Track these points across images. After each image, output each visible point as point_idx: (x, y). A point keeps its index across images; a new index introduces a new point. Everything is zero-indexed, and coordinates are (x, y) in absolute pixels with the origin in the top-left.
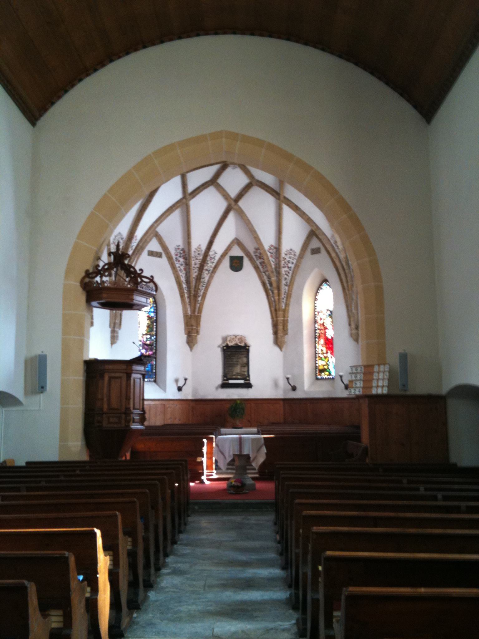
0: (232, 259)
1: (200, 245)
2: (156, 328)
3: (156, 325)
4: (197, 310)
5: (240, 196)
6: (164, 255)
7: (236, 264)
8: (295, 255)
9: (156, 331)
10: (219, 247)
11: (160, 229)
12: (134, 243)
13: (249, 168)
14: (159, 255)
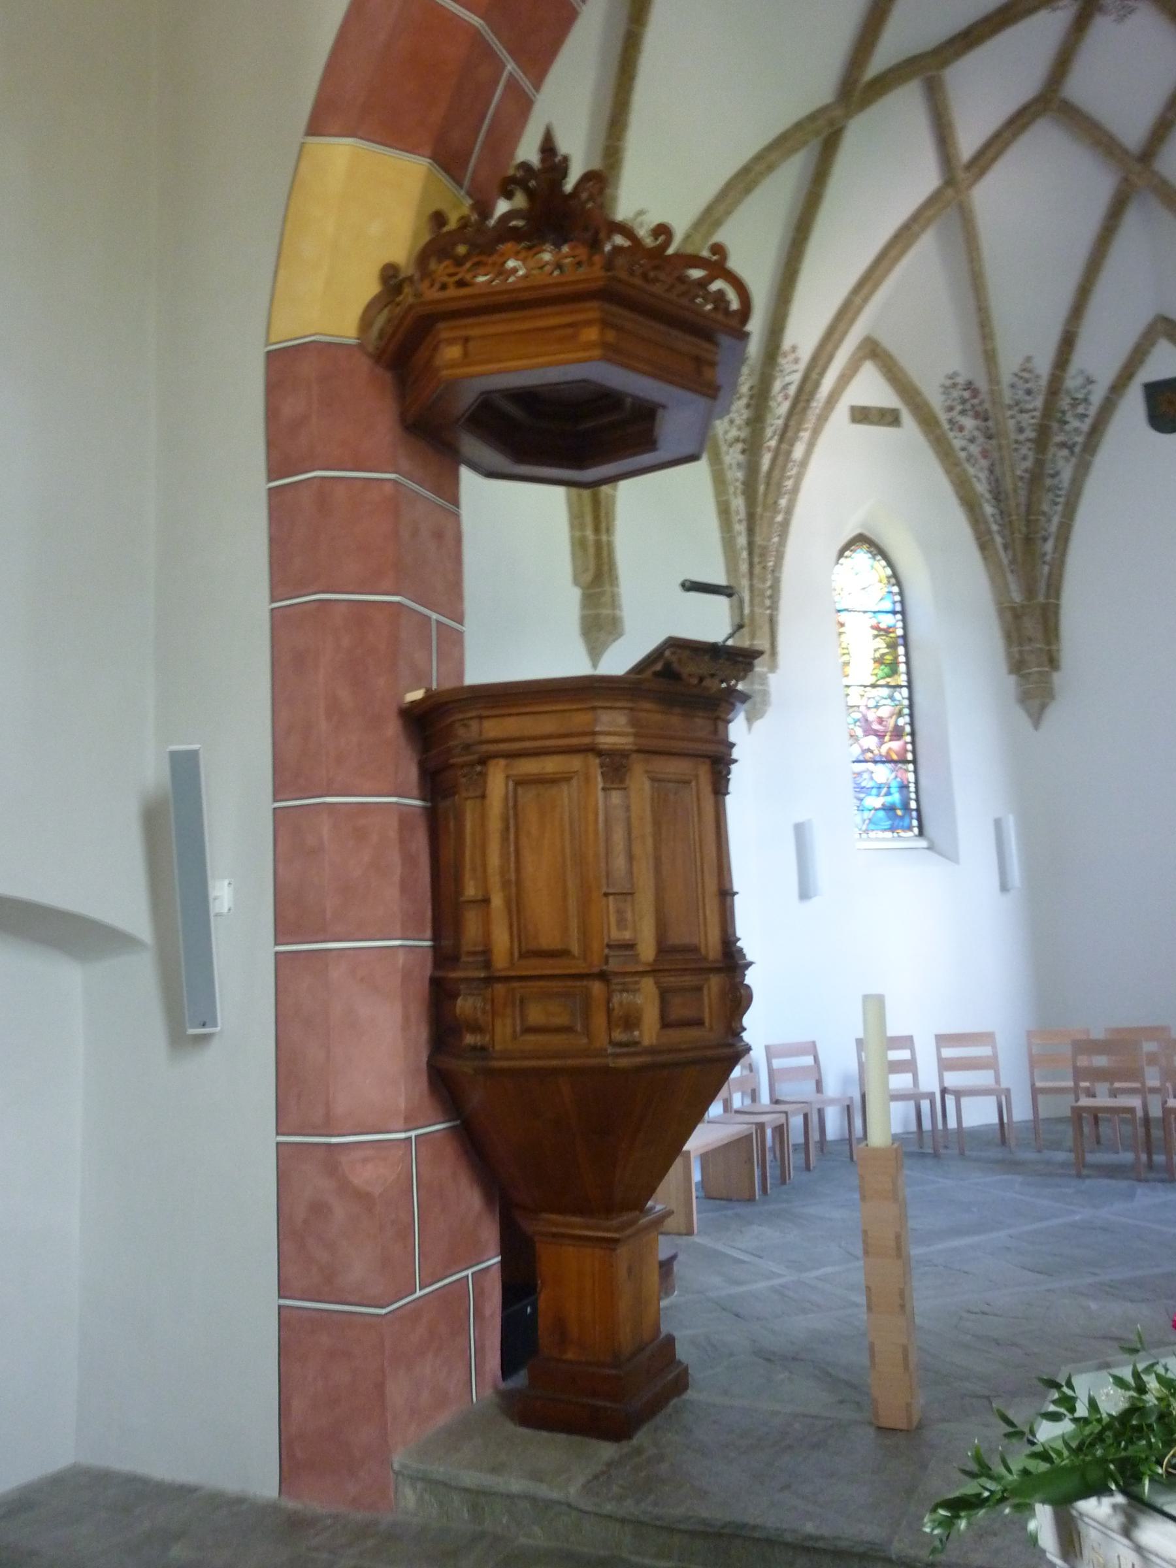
1: (1029, 359)
2: (907, 663)
3: (907, 655)
4: (1042, 585)
6: (906, 417)
9: (908, 673)
10: (1098, 359)
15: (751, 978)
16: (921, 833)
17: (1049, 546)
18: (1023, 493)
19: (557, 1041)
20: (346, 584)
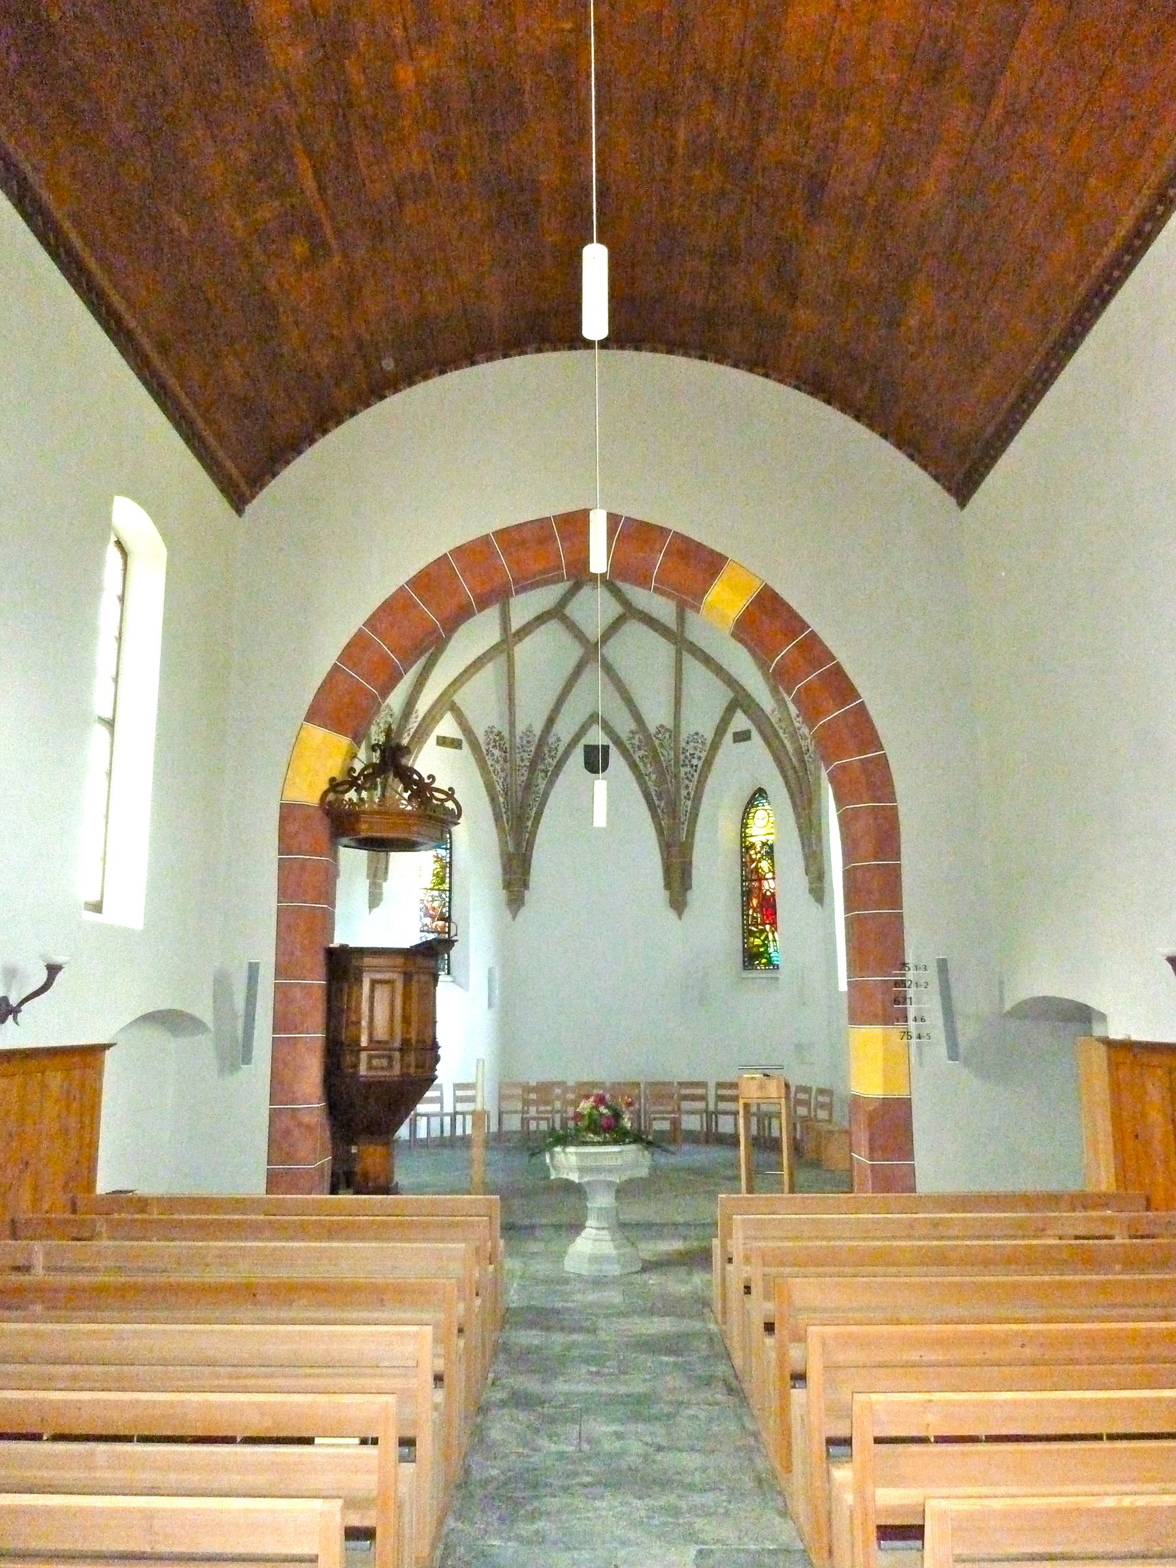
0: (590, 751)
5: (607, 635)
6: (465, 744)
7: (595, 761)
8: (703, 743)
10: (564, 730)
11: (458, 698)
12: (413, 724)
13: (620, 584)
14: (456, 744)
15: (440, 1052)
16: (449, 973)
17: (529, 824)
18: (520, 794)
19: (380, 1073)
20: (305, 896)
